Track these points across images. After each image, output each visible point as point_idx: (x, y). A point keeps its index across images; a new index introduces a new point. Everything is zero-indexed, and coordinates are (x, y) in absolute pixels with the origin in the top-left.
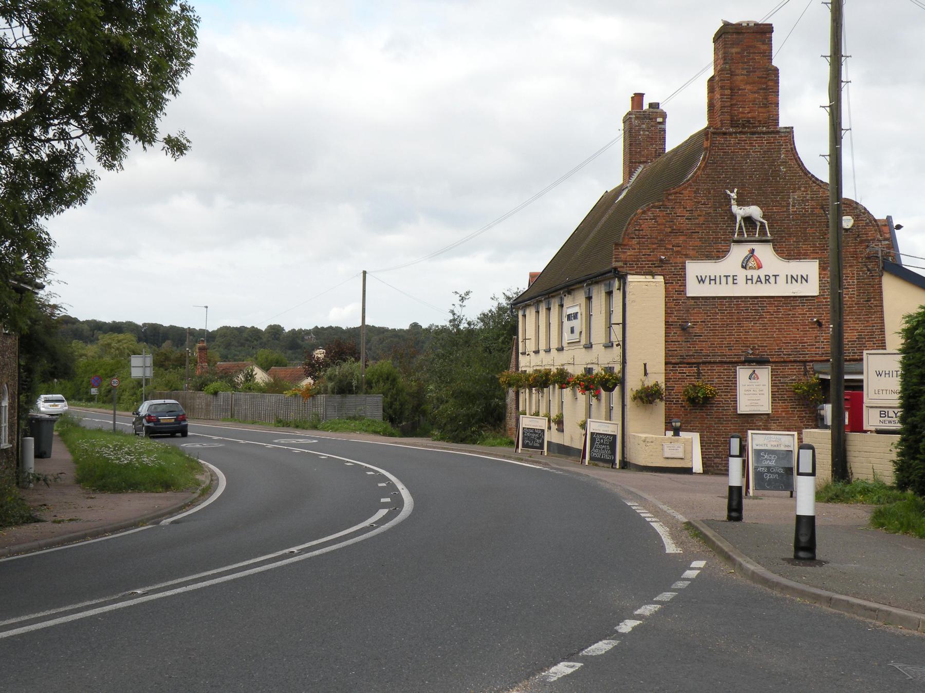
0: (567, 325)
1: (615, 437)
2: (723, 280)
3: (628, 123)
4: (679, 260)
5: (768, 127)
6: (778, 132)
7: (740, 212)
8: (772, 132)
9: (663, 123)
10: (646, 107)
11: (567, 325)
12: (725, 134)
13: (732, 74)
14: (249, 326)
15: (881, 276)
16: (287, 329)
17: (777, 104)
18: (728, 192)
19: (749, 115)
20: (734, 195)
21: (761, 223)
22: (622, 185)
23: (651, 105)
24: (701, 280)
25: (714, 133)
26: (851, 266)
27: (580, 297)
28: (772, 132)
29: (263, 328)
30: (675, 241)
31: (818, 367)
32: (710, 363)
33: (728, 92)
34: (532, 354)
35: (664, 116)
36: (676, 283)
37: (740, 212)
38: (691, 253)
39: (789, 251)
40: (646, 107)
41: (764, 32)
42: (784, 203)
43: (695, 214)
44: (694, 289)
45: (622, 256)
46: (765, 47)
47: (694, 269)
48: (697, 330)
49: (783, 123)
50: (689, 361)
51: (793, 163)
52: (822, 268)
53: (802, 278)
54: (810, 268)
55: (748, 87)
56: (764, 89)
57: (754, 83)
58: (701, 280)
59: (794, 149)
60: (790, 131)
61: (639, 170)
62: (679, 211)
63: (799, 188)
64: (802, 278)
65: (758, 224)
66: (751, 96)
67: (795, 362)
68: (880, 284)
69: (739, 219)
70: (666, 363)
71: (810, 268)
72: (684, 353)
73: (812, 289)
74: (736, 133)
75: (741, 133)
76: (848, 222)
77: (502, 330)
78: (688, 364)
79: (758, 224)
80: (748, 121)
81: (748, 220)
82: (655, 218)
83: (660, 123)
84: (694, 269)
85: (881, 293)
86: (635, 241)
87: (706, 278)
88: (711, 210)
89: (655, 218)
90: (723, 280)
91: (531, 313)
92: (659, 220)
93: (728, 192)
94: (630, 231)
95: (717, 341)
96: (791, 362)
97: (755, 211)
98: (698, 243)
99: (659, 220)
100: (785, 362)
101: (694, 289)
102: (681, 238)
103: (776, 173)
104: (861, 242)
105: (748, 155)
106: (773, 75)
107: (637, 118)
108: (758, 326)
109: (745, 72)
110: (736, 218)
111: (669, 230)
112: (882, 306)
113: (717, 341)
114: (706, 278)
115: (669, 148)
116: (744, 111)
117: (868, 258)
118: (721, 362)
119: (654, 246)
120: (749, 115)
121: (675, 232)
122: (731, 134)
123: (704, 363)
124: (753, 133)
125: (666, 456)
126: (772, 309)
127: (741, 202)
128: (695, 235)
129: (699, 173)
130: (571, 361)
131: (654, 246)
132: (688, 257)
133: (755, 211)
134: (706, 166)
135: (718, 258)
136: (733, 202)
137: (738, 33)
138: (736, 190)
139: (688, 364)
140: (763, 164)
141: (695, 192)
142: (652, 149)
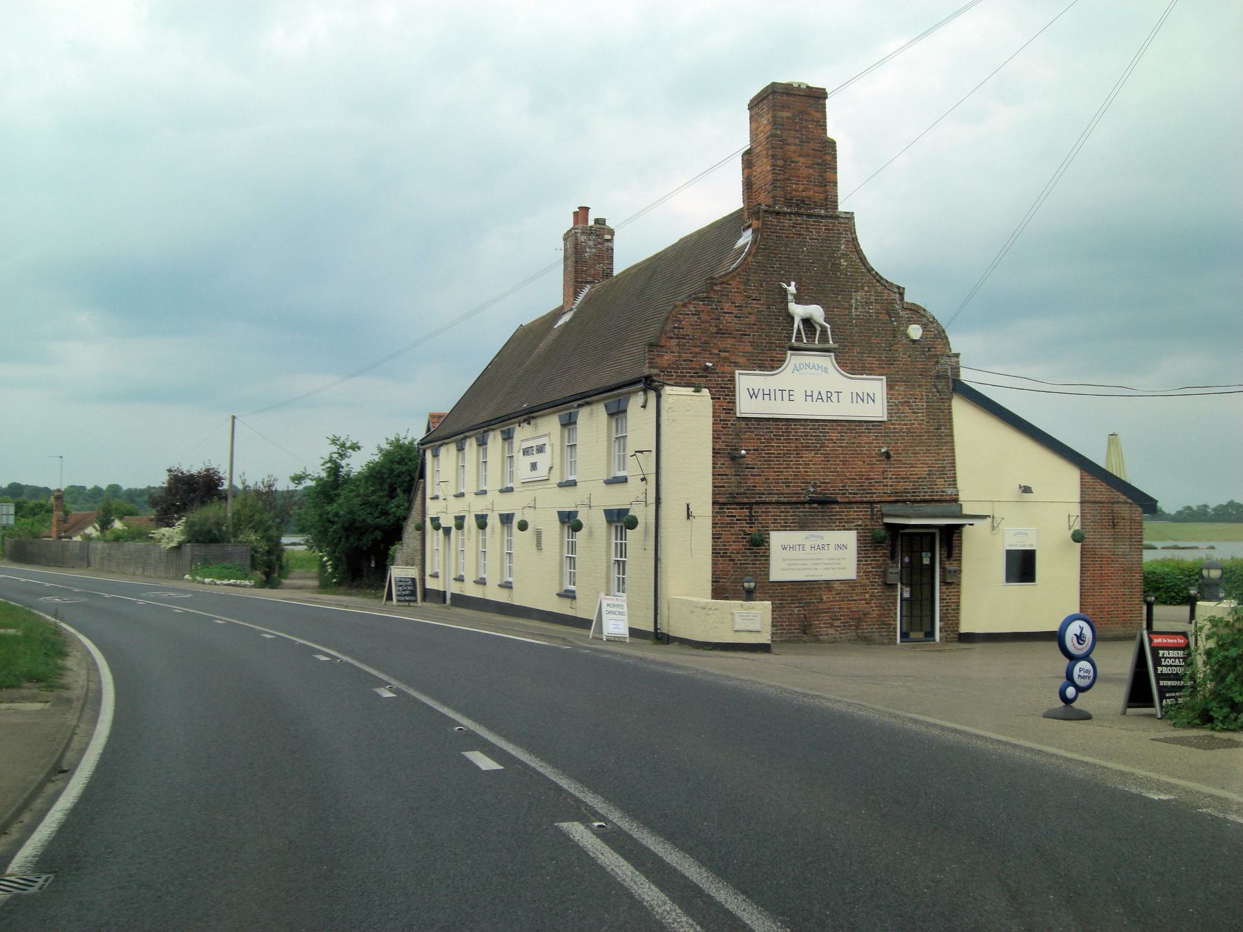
0: (523, 463)
1: (413, 580)
2: (779, 394)
3: (572, 239)
4: (727, 369)
5: (826, 210)
6: (837, 217)
7: (799, 311)
8: (831, 217)
9: (610, 241)
10: (591, 223)
11: (523, 463)
12: (778, 213)
13: (785, 143)
14: (89, 486)
15: (950, 400)
16: (125, 488)
17: (835, 183)
18: (785, 285)
19: (804, 194)
20: (792, 289)
21: (821, 326)
22: (562, 307)
23: (597, 221)
24: (753, 395)
25: (766, 211)
26: (920, 386)
27: (550, 426)
28: (831, 217)
29: (104, 487)
30: (722, 345)
31: (886, 509)
32: (765, 503)
33: (780, 163)
34: (451, 499)
35: (612, 232)
36: (724, 395)
37: (799, 311)
38: (741, 360)
39: (852, 365)
40: (591, 223)
41: (817, 97)
42: (846, 305)
43: (746, 311)
44: (746, 406)
45: (658, 360)
46: (818, 115)
47: (746, 382)
48: (748, 460)
49: (842, 208)
50: (740, 500)
51: (854, 256)
52: (890, 387)
53: (861, 398)
54: (876, 386)
55: (802, 160)
56: (819, 164)
57: (808, 156)
58: (753, 395)
59: (855, 239)
60: (850, 217)
61: (586, 290)
62: (727, 306)
63: (863, 287)
64: (861, 398)
65: (818, 329)
66: (804, 171)
67: (862, 502)
68: (950, 408)
69: (797, 322)
70: (714, 503)
71: (876, 386)
72: (734, 490)
73: (877, 411)
74: (790, 213)
75: (797, 214)
76: (915, 332)
77: (401, 474)
78: (738, 504)
79: (818, 329)
80: (803, 201)
81: (807, 322)
82: (697, 314)
83: (608, 240)
84: (746, 382)
85: (951, 419)
86: (674, 342)
87: (760, 394)
88: (763, 308)
89: (697, 314)
90: (779, 394)
91: (448, 453)
92: (703, 316)
93: (785, 285)
94: (667, 328)
95: (772, 475)
96: (856, 502)
97: (816, 312)
98: (749, 349)
99: (703, 316)
100: (850, 503)
101: (746, 406)
102: (730, 341)
103: (836, 266)
104: (930, 357)
105: (804, 243)
106: (829, 147)
107: (583, 233)
108: (820, 457)
109: (797, 141)
110: (793, 318)
111: (715, 330)
112: (952, 436)
113: (772, 475)
114: (760, 394)
115: (615, 274)
116: (798, 189)
117: (938, 377)
118: (778, 503)
119: (697, 350)
120: (804, 194)
121: (721, 333)
122: (785, 214)
123: (757, 503)
124: (809, 216)
125: (737, 628)
126: (834, 436)
127: (799, 300)
128: (746, 339)
129: (750, 259)
130: (586, 502)
131: (697, 350)
132: (737, 365)
133: (816, 312)
134: (757, 252)
135: (773, 368)
136: (790, 297)
137: (788, 94)
138: (793, 283)
139: (738, 504)
140: (821, 255)
141: (745, 284)
142: (599, 267)
